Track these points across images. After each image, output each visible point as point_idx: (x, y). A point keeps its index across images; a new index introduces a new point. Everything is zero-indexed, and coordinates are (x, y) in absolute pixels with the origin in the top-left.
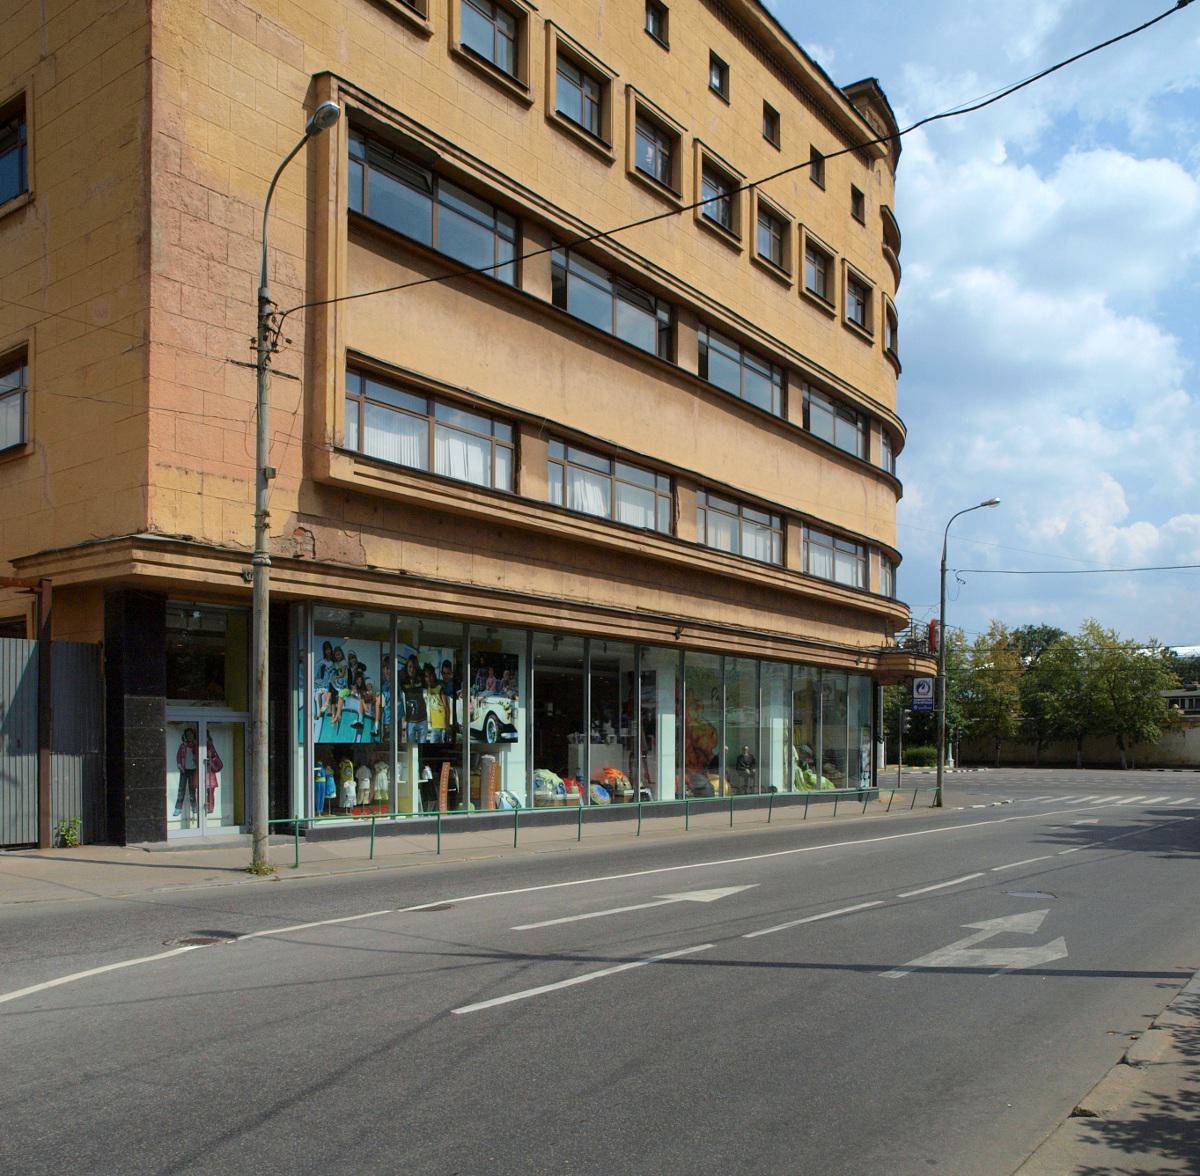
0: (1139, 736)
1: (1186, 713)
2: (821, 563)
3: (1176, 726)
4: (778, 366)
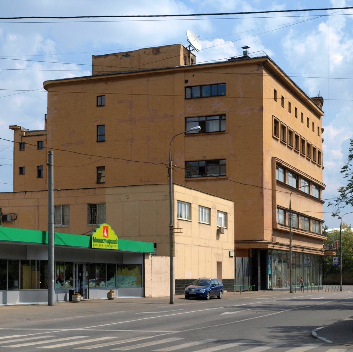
4: (306, 179)
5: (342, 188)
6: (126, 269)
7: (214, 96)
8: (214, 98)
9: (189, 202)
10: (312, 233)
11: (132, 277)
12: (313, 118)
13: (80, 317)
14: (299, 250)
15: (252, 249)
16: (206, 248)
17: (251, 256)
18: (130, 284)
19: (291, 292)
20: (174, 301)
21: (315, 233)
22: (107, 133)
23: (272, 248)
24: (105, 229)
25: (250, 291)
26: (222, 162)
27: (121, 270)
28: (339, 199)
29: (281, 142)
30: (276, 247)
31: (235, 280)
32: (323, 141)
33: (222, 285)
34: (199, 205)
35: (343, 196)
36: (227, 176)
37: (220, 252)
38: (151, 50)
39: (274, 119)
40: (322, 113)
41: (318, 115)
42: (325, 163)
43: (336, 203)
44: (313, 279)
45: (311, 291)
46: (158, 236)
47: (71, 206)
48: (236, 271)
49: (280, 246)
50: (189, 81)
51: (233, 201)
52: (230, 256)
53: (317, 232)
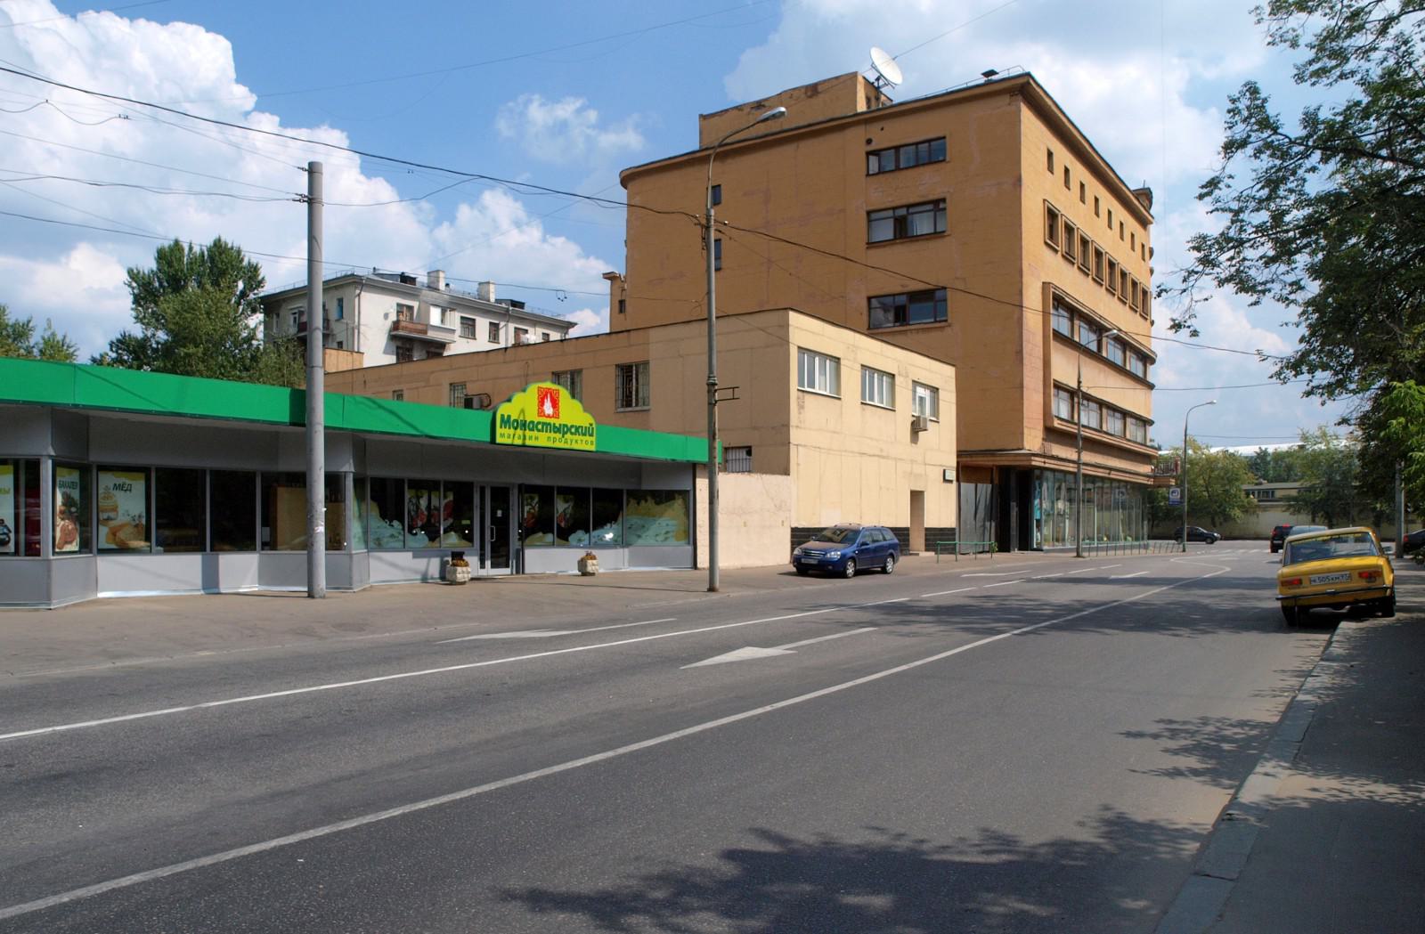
0: (1228, 518)
1: (1259, 501)
2: (1113, 425)
3: (1252, 510)
5: (1204, 238)
6: (650, 503)
7: (923, 165)
8: (921, 170)
9: (834, 355)
10: (1129, 440)
11: (669, 518)
12: (1131, 224)
13: (59, 671)
14: (1101, 473)
16: (882, 460)
17: (996, 482)
18: (660, 538)
19: (1078, 556)
20: (717, 584)
21: (1135, 442)
23: (1042, 465)
24: (546, 395)
26: (938, 294)
27: (638, 503)
28: (1191, 272)
29: (1063, 256)
30: (1051, 464)
31: (957, 531)
32: (1152, 272)
33: (896, 541)
34: (862, 365)
35: (1207, 261)
36: (949, 321)
37: (918, 469)
38: (803, 90)
39: (1048, 208)
40: (1150, 218)
41: (1144, 222)
43: (1184, 286)
44: (1130, 529)
45: (1122, 552)
46: (755, 428)
47: (584, 371)
48: (978, 516)
49: (1059, 463)
50: (874, 139)
51: (953, 365)
52: (945, 480)
53: (1139, 439)
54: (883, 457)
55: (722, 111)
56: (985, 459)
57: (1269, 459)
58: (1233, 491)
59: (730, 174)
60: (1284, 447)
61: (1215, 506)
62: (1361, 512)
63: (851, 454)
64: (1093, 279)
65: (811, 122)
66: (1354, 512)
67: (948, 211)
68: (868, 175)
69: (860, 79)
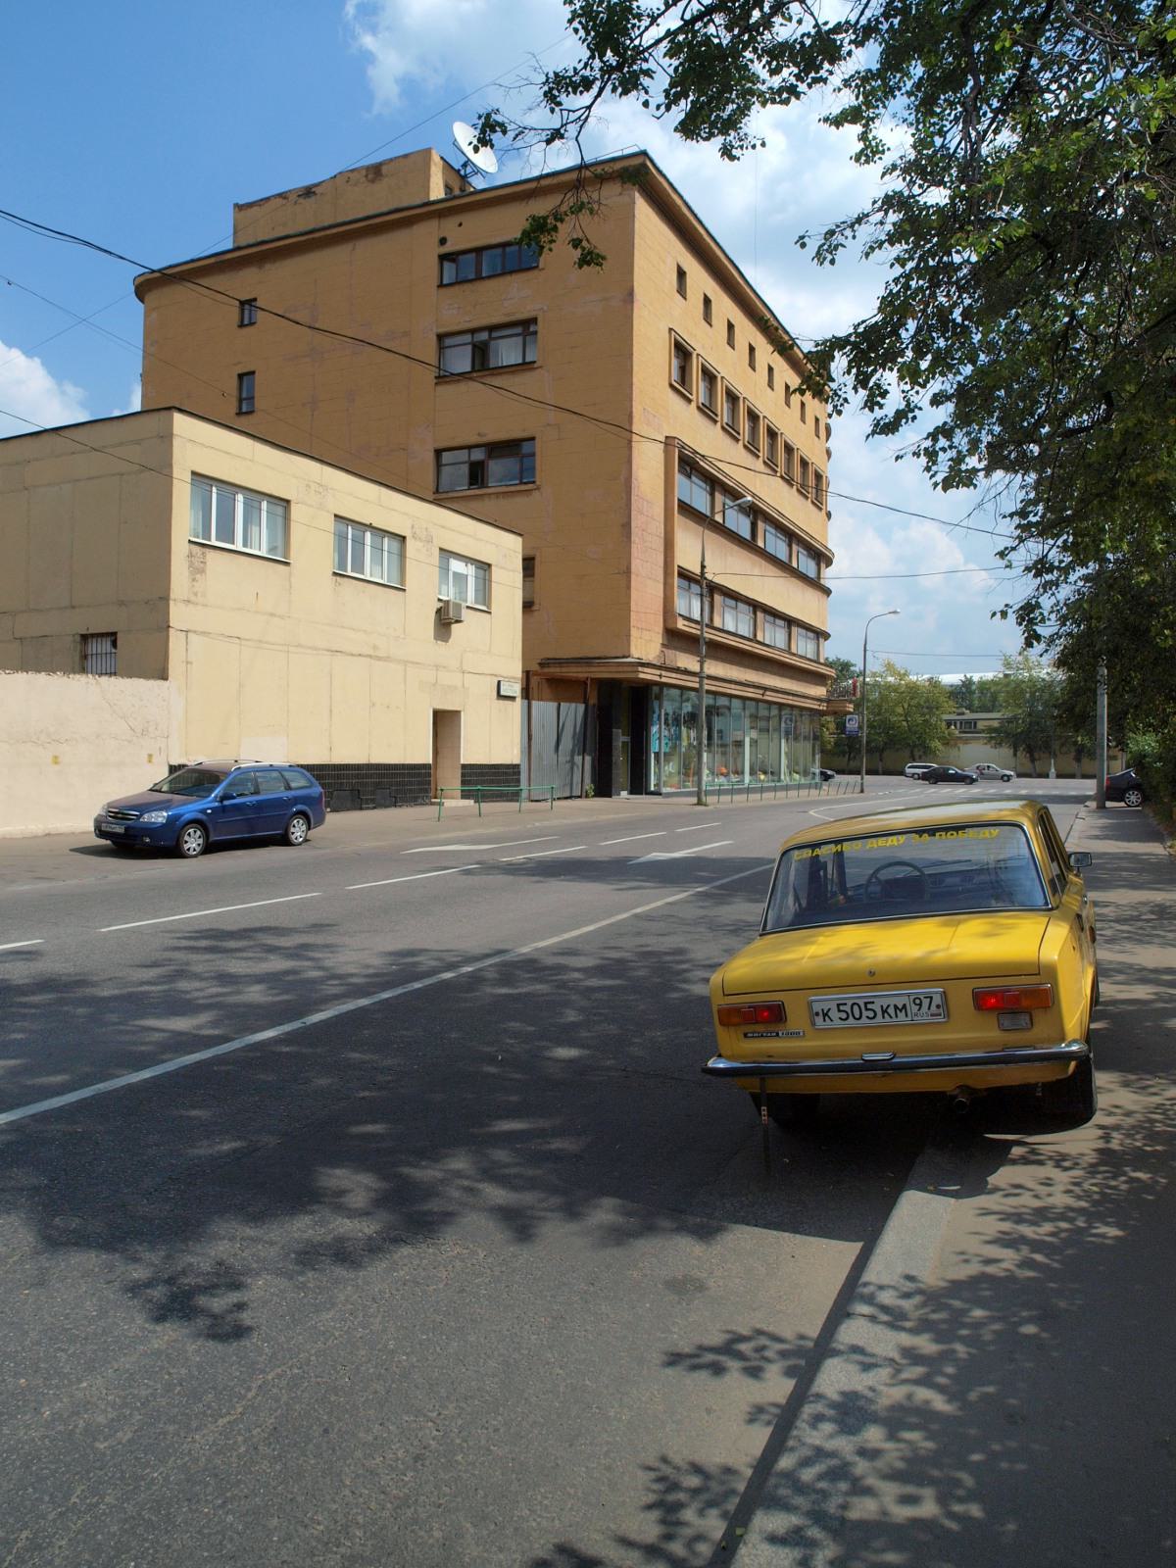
2: (773, 636)
7: (511, 272)
8: (508, 278)
10: (794, 655)
14: (750, 693)
15: (592, 679)
19: (699, 803)
22: (259, 393)
23: (657, 679)
25: (587, 796)
26: (526, 448)
29: (723, 428)
38: (364, 172)
42: (832, 503)
51: (520, 535)
54: (379, 658)
55: (261, 200)
56: (580, 669)
57: (974, 687)
58: (933, 720)
59: (263, 283)
60: (989, 676)
61: (914, 738)
62: (1062, 745)
63: (309, 651)
64: (813, 502)
65: (371, 212)
66: (1056, 746)
67: (539, 334)
68: (441, 285)
69: (436, 158)
